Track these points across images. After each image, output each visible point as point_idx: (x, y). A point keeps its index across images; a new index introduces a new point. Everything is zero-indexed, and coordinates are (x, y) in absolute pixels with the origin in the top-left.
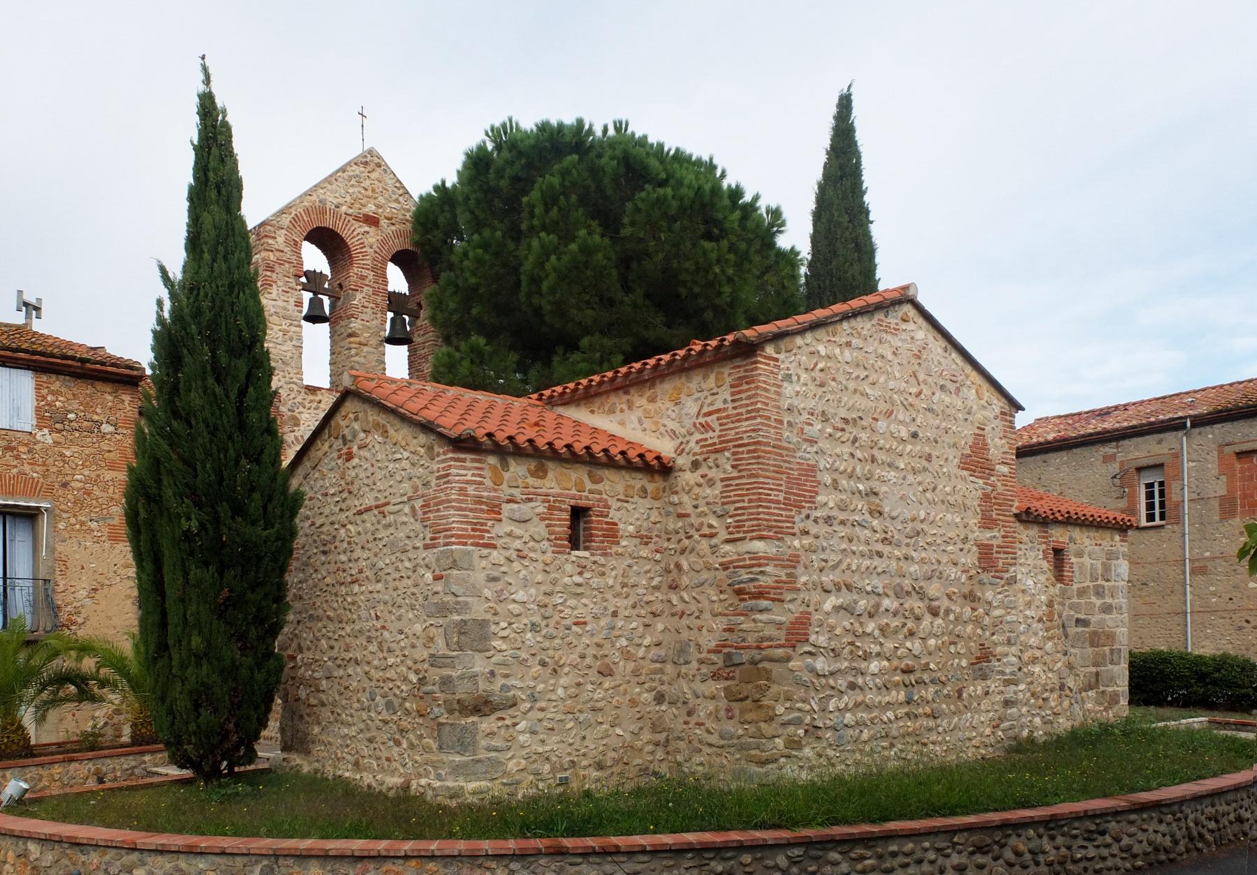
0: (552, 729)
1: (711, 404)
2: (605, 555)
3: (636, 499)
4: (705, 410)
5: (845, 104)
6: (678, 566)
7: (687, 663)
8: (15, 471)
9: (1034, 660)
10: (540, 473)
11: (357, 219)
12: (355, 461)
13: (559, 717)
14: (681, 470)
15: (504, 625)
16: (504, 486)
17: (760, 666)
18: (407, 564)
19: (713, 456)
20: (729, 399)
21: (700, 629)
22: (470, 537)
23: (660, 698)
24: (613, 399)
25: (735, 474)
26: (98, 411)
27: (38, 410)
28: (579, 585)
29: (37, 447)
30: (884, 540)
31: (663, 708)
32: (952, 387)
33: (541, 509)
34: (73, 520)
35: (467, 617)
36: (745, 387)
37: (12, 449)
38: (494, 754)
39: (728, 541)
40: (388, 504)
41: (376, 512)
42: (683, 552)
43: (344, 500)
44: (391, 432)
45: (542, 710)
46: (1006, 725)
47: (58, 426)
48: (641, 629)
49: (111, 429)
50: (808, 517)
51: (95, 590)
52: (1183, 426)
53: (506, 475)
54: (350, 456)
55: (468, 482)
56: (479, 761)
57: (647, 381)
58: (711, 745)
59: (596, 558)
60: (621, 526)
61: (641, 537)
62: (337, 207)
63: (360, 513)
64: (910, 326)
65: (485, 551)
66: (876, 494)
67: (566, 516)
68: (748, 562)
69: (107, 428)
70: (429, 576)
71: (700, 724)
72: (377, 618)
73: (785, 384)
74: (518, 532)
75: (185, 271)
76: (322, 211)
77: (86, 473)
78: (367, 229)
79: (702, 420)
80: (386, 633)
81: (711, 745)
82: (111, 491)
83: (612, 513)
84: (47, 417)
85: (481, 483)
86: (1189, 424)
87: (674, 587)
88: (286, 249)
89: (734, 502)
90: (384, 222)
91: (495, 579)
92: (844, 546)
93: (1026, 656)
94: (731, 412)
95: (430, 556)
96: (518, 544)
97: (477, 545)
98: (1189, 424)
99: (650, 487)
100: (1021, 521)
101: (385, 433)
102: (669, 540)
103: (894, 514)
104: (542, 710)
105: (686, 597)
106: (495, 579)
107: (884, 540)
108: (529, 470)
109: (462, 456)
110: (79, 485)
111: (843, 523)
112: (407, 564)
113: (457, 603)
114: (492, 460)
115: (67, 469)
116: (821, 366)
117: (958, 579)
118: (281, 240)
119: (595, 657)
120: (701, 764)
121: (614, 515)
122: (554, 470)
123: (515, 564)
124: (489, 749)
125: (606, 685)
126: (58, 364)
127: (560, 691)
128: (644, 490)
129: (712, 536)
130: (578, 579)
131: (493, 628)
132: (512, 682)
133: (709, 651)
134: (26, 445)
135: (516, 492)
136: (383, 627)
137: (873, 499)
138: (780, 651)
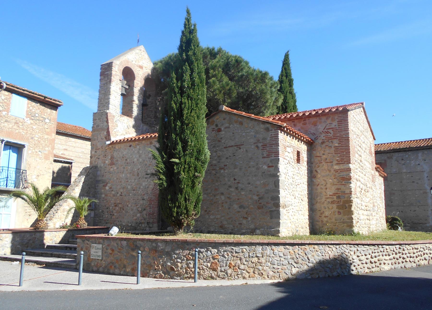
4: (327, 127)
5: (287, 57)
8: (17, 131)
11: (137, 66)
19: (330, 140)
20: (337, 125)
26: (45, 114)
27: (27, 111)
29: (25, 124)
34: (34, 151)
36: (343, 122)
37: (17, 123)
41: (236, 147)
47: (33, 118)
51: (38, 176)
54: (219, 130)
65: (284, 160)
69: (47, 121)
70: (265, 167)
72: (235, 179)
75: (151, 72)
76: (128, 62)
77: (39, 135)
78: (140, 69)
79: (326, 131)
84: (30, 115)
90: (144, 68)
115: (33, 133)
118: (117, 68)
126: (36, 97)
134: (22, 123)
136: (239, 183)
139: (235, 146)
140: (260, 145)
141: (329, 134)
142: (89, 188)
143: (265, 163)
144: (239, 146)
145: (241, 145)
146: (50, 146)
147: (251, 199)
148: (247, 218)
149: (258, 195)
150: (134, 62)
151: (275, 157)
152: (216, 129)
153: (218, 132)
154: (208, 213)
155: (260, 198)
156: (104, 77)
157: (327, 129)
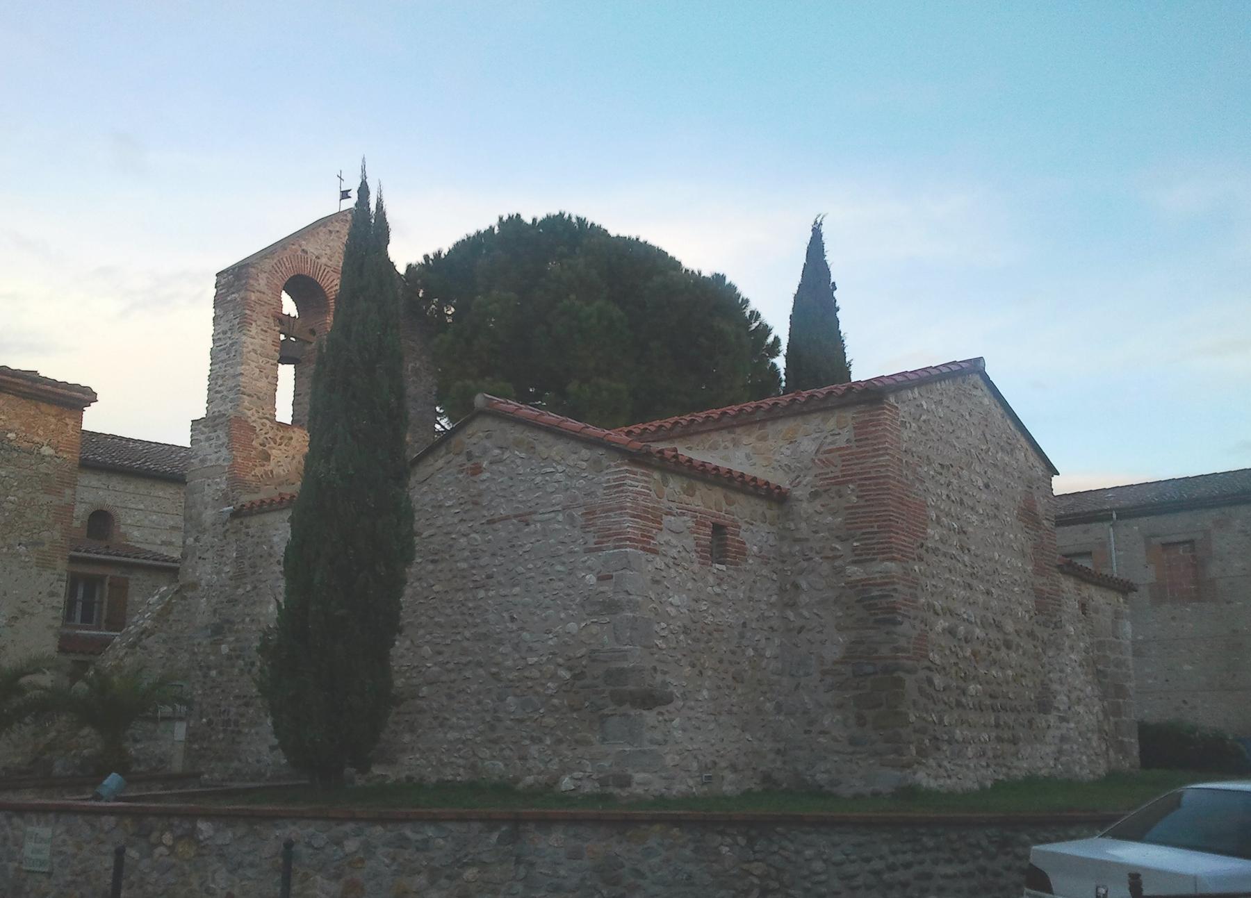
0: (699, 728)
1: (833, 443)
2: (736, 570)
3: (758, 523)
6: (796, 586)
7: (807, 674)
9: (1079, 700)
10: (690, 492)
12: (485, 476)
13: (704, 717)
14: (798, 500)
15: (663, 625)
16: (664, 500)
17: (895, 675)
18: (559, 568)
19: (835, 488)
21: (823, 643)
22: (639, 541)
23: (779, 708)
24: (715, 437)
25: (862, 503)
26: (41, 433)
28: (718, 595)
30: (972, 575)
31: (782, 718)
32: (1008, 448)
33: (690, 524)
35: (637, 614)
38: (655, 747)
39: (855, 563)
40: (535, 513)
42: (801, 572)
43: (466, 512)
44: (540, 448)
45: (692, 709)
46: (1063, 759)
48: (763, 641)
49: (52, 452)
50: (922, 545)
52: (1110, 518)
53: (667, 490)
54: (477, 470)
55: (639, 493)
56: (644, 752)
57: (756, 422)
58: (838, 752)
59: (731, 572)
60: (748, 545)
61: (762, 557)
62: (317, 257)
63: (490, 522)
64: (978, 393)
65: (650, 556)
66: (965, 533)
67: (708, 531)
68: (879, 581)
70: (591, 578)
71: (823, 733)
72: (513, 619)
73: (903, 430)
74: (674, 542)
79: (823, 457)
80: (526, 635)
81: (838, 752)
82: (44, 516)
83: (742, 533)
85: (648, 495)
86: (1114, 516)
87: (793, 605)
88: (266, 291)
89: (861, 528)
91: (657, 582)
92: (947, 576)
93: (1074, 696)
94: (855, 450)
95: (592, 560)
96: (674, 552)
97: (643, 549)
98: (1114, 516)
99: (769, 513)
100: (1063, 573)
101: (531, 448)
102: (784, 562)
103: (978, 553)
104: (692, 709)
105: (806, 613)
106: (657, 582)
107: (972, 575)
108: (682, 488)
109: (635, 469)
110: (11, 506)
111: (945, 555)
112: (559, 568)
113: (630, 601)
114: (657, 475)
116: (924, 417)
117: (1023, 617)
118: (263, 282)
119: (730, 662)
120: (827, 771)
121: (744, 535)
122: (701, 489)
123: (672, 571)
124: (652, 742)
125: (740, 691)
127: (705, 693)
128: (764, 514)
129: (835, 558)
130: (718, 590)
131: (656, 627)
132: (668, 679)
133: (835, 663)
135: (673, 505)
136: (522, 629)
137: (963, 536)
138: (910, 662)
139: (515, 516)
140: (577, 513)
141: (833, 468)
142: (171, 651)
143: (590, 569)
144: (524, 519)
145: (530, 513)
146: (58, 526)
147: (554, 677)
148: (541, 741)
149: (570, 669)
150: (324, 260)
151: (615, 548)
152: (469, 465)
153: (473, 475)
154: (441, 725)
155: (575, 677)
156: (226, 312)
157: (825, 452)
